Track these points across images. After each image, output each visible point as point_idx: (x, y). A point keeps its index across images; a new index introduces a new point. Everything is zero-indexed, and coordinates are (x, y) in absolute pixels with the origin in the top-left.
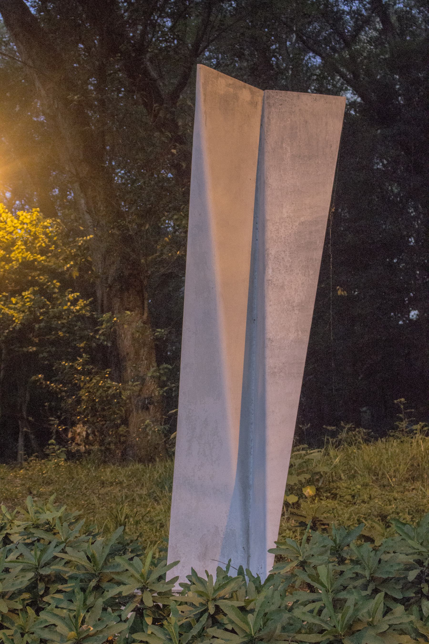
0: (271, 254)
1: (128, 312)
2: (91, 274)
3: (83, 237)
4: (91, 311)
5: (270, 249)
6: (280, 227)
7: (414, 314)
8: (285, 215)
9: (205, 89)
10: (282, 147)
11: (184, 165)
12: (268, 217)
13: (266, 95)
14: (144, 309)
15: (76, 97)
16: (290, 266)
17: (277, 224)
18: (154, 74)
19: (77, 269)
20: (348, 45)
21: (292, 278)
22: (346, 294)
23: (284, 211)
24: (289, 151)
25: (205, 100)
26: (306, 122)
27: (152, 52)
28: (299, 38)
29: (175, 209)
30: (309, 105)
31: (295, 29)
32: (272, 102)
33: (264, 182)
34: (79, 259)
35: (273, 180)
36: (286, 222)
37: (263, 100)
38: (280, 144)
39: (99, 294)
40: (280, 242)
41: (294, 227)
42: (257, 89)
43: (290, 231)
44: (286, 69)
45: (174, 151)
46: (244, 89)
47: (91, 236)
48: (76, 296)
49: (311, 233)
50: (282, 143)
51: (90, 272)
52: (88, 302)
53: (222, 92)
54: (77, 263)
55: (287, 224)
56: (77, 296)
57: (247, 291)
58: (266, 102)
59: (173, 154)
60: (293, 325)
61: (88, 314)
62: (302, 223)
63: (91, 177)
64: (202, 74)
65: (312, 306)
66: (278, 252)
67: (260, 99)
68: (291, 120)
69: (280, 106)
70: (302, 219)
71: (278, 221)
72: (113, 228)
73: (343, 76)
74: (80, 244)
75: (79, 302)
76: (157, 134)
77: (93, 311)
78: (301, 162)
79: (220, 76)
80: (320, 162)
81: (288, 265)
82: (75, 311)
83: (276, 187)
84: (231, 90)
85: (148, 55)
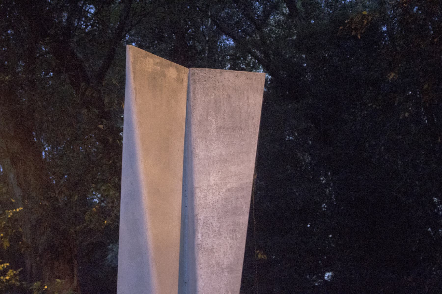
0: (200, 219)
1: (58, 280)
2: (22, 244)
3: (12, 210)
4: (20, 281)
5: (199, 215)
6: (208, 194)
7: (328, 275)
8: (212, 183)
9: (134, 68)
10: (207, 120)
11: (110, 139)
12: (196, 185)
13: (191, 73)
14: (73, 277)
15: (7, 78)
16: (219, 231)
17: (206, 191)
18: (80, 56)
19: (7, 239)
20: (258, 28)
21: (220, 241)
22: (266, 258)
23: (211, 179)
24: (214, 123)
25: (134, 78)
26: (229, 97)
27: (78, 35)
28: (214, 22)
29: (103, 180)
30: (231, 80)
31: (210, 14)
32: (196, 78)
33: (192, 153)
34: (10, 230)
35: (200, 151)
36: (213, 189)
37: (189, 77)
38: (205, 117)
39: (28, 263)
40: (208, 208)
41: (221, 194)
42: (183, 67)
43: (217, 198)
44: (203, 50)
45: (101, 126)
46: (171, 68)
47: (21, 208)
48: (5, 267)
49: (237, 198)
50: (207, 116)
51: (20, 243)
52: (18, 272)
53: (151, 71)
54: (8, 235)
55: (214, 191)
56: (7, 266)
57: (178, 255)
58: (191, 79)
59: (100, 130)
60: (223, 286)
61: (18, 284)
62: (229, 190)
63: (22, 152)
64: (131, 54)
65: (241, 268)
66: (206, 217)
67: (185, 77)
68: (215, 95)
69: (204, 83)
70: (229, 186)
71: (206, 188)
72: (43, 200)
73: (254, 56)
74: (9, 216)
75: (9, 272)
76: (84, 111)
77: (23, 281)
78: (225, 134)
79: (148, 56)
80: (243, 133)
81: (217, 229)
82: (4, 281)
83: (203, 157)
84: (159, 68)
85: (75, 39)
